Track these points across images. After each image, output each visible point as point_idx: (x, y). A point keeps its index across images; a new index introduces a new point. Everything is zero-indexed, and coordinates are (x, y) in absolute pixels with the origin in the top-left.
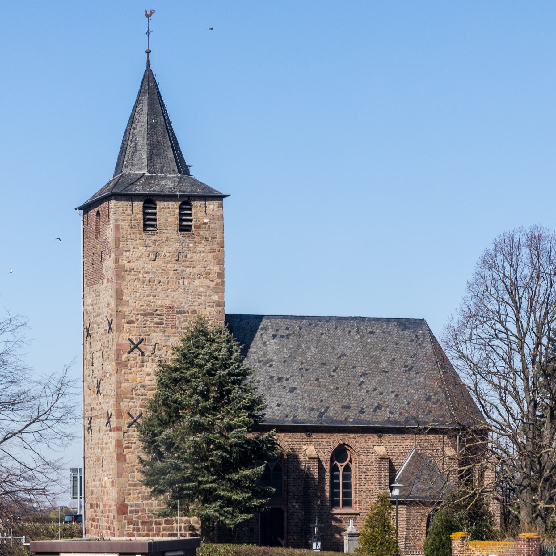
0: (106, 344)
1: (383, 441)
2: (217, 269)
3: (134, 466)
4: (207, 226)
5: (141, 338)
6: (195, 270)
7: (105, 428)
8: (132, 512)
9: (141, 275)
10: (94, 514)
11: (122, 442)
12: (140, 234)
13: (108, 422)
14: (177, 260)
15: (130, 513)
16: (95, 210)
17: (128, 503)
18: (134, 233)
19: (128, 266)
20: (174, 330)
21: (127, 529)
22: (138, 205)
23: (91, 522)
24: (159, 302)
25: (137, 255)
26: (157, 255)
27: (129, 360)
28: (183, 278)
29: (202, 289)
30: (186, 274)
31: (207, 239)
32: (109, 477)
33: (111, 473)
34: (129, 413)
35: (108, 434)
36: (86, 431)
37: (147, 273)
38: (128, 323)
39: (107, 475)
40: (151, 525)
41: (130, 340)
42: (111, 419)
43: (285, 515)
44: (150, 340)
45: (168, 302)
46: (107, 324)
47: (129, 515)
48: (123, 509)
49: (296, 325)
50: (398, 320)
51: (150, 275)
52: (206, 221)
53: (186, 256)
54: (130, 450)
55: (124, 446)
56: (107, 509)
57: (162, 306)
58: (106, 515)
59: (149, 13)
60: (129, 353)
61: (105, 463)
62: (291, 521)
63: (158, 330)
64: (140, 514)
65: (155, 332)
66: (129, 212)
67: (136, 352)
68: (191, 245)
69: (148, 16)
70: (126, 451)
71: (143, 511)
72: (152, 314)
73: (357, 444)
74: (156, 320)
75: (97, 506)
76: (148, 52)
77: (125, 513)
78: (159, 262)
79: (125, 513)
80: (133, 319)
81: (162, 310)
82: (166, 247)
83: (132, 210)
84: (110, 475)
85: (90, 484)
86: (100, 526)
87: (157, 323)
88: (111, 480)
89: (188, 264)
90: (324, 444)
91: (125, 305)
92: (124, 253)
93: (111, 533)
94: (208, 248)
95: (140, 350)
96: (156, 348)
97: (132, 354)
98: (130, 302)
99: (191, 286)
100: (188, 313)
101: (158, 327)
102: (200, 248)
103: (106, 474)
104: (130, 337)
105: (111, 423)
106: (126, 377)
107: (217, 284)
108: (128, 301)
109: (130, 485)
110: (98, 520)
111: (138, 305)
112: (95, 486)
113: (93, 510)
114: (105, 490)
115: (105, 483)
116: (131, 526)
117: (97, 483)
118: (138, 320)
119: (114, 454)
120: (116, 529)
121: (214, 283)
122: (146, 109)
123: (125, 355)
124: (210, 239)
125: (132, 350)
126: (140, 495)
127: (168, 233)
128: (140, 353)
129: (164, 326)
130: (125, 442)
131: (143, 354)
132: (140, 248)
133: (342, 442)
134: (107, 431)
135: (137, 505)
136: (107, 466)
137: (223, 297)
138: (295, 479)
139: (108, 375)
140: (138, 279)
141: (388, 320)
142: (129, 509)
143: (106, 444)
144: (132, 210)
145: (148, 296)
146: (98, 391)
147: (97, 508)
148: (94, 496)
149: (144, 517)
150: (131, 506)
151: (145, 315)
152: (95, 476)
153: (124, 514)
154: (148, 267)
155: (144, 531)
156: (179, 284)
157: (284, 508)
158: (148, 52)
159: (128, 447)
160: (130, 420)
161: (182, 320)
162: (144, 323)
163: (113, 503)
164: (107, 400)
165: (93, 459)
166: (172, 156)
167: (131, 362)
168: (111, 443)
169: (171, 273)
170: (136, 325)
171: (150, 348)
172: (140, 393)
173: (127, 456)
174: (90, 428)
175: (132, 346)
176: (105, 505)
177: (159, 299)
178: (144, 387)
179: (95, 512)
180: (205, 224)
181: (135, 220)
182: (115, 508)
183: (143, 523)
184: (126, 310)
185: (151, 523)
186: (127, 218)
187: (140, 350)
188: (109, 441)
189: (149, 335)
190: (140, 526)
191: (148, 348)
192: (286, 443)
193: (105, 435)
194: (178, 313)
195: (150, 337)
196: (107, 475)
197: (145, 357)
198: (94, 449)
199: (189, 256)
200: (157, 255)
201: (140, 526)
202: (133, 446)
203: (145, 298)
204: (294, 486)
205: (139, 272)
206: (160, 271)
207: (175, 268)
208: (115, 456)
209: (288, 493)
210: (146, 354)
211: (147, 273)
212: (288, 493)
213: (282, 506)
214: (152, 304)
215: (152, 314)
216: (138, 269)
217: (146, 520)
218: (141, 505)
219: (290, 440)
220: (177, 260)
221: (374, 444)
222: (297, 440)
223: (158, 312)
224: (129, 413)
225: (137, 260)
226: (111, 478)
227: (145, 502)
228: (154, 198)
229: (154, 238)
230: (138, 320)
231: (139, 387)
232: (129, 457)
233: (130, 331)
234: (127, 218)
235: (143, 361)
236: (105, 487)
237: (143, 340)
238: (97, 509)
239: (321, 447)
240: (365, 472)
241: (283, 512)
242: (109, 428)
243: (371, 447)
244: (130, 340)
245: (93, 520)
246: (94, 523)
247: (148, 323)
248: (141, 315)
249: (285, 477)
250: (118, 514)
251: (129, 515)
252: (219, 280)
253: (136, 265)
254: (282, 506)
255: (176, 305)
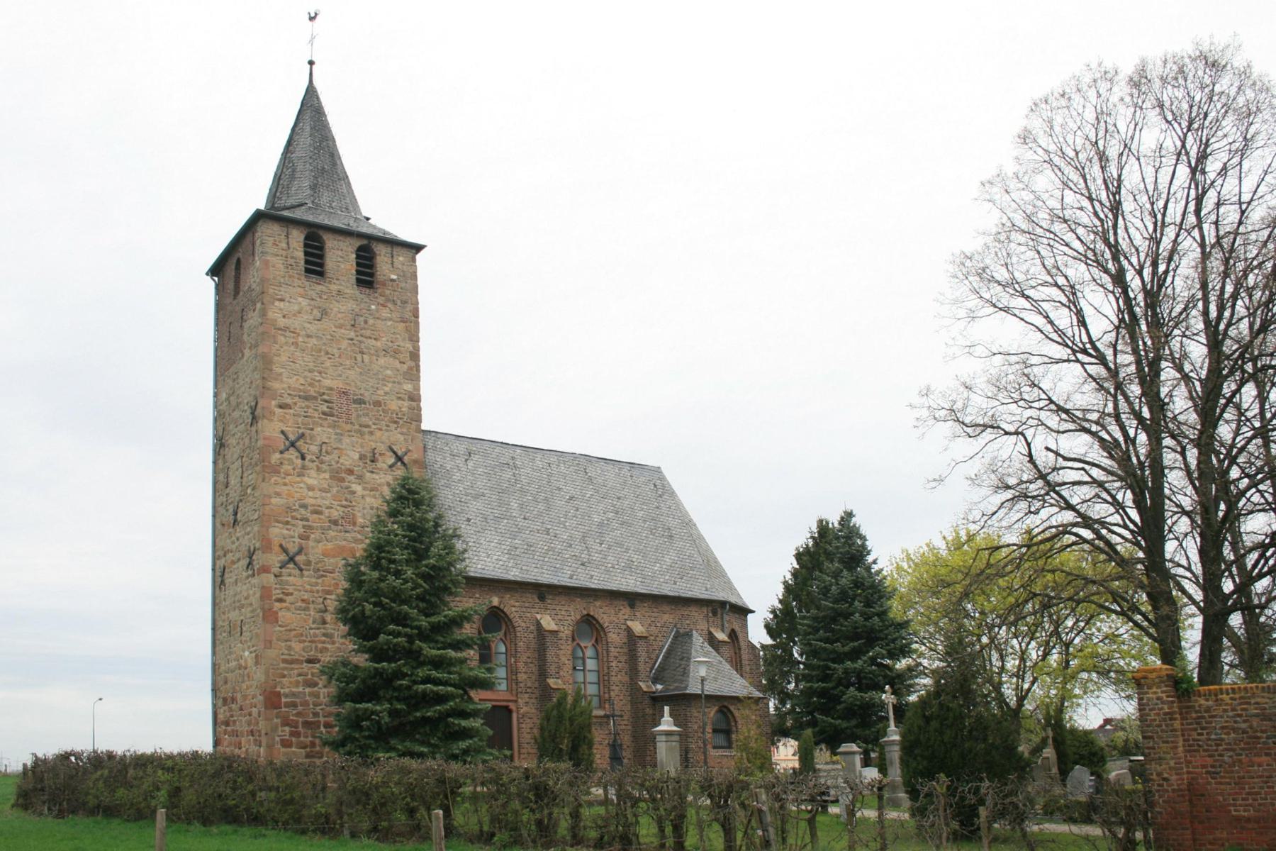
1: (637, 613)
2: (409, 346)
3: (290, 630)
4: (395, 284)
6: (379, 344)
7: (245, 574)
8: (287, 705)
9: (301, 339)
11: (271, 591)
12: (299, 279)
13: (250, 564)
14: (353, 326)
15: (285, 707)
17: (282, 691)
18: (290, 276)
19: (282, 322)
20: (349, 427)
22: (298, 237)
23: (224, 727)
24: (327, 383)
26: (324, 313)
27: (281, 463)
28: (362, 353)
29: (389, 372)
30: (366, 348)
31: (394, 302)
34: (281, 546)
36: (217, 589)
37: (309, 336)
38: (281, 407)
39: (249, 648)
40: (319, 727)
41: (283, 432)
42: (254, 557)
43: (515, 716)
44: (312, 437)
47: (284, 709)
51: (314, 341)
52: (394, 277)
53: (366, 322)
54: (284, 605)
57: (331, 389)
59: (313, 15)
60: (281, 452)
61: (244, 629)
62: (523, 726)
63: (325, 423)
64: (300, 708)
65: (321, 425)
66: (284, 245)
68: (373, 307)
69: (312, 19)
70: (277, 605)
71: (305, 704)
72: (315, 398)
73: (605, 616)
74: (324, 408)
75: (233, 700)
76: (311, 63)
77: (278, 706)
78: (326, 323)
79: (278, 706)
80: (289, 401)
82: (337, 305)
83: (288, 244)
85: (223, 668)
87: (324, 413)
88: (254, 655)
89: (368, 333)
90: (563, 613)
91: (276, 379)
92: (277, 303)
93: (256, 740)
95: (299, 451)
96: (324, 450)
97: (286, 455)
98: (285, 375)
99: (373, 366)
103: (246, 646)
104: (284, 429)
107: (410, 368)
108: (281, 374)
109: (285, 661)
110: (234, 722)
111: (295, 382)
113: (226, 708)
114: (246, 672)
115: (246, 661)
116: (287, 729)
118: (295, 404)
119: (259, 611)
120: (263, 732)
121: (405, 366)
122: (308, 129)
123: (277, 456)
124: (399, 303)
126: (300, 679)
127: (341, 285)
128: (297, 454)
130: (278, 591)
132: (300, 299)
133: (585, 612)
136: (248, 634)
137: (417, 388)
138: (526, 663)
140: (295, 344)
142: (284, 700)
144: (288, 244)
148: (229, 685)
151: (306, 398)
152: (230, 653)
153: (276, 708)
154: (312, 328)
155: (307, 737)
156: (356, 360)
157: (512, 706)
158: (311, 63)
159: (280, 600)
160: (283, 557)
161: (361, 413)
163: (258, 692)
164: (249, 529)
165: (227, 628)
167: (286, 467)
170: (292, 411)
171: (314, 449)
172: (299, 517)
173: (280, 614)
174: (222, 582)
176: (245, 697)
178: (304, 506)
180: (393, 280)
181: (292, 258)
182: (261, 698)
183: (307, 724)
184: (276, 385)
186: (281, 252)
189: (312, 429)
190: (300, 729)
192: (513, 609)
194: (355, 402)
197: (307, 463)
199: (371, 321)
200: (324, 313)
201: (300, 729)
202: (289, 599)
203: (306, 373)
204: (525, 673)
205: (299, 335)
206: (329, 337)
207: (350, 337)
208: (261, 614)
209: (517, 684)
210: (308, 457)
212: (517, 684)
213: (510, 704)
215: (315, 398)
217: (311, 719)
219: (517, 604)
220: (353, 326)
221: (626, 617)
222: (527, 605)
224: (281, 546)
225: (294, 315)
227: (307, 690)
228: (321, 233)
229: (319, 288)
230: (295, 404)
231: (297, 507)
234: (281, 252)
235: (303, 467)
236: (246, 668)
237: (303, 435)
238: (234, 706)
239: (560, 617)
240: (616, 657)
241: (510, 711)
243: (623, 621)
244: (283, 432)
245: (227, 724)
246: (229, 729)
247: (310, 410)
248: (300, 397)
249: (513, 660)
250: (266, 708)
251: (284, 709)
252: (413, 364)
253: (295, 323)
254: (510, 704)
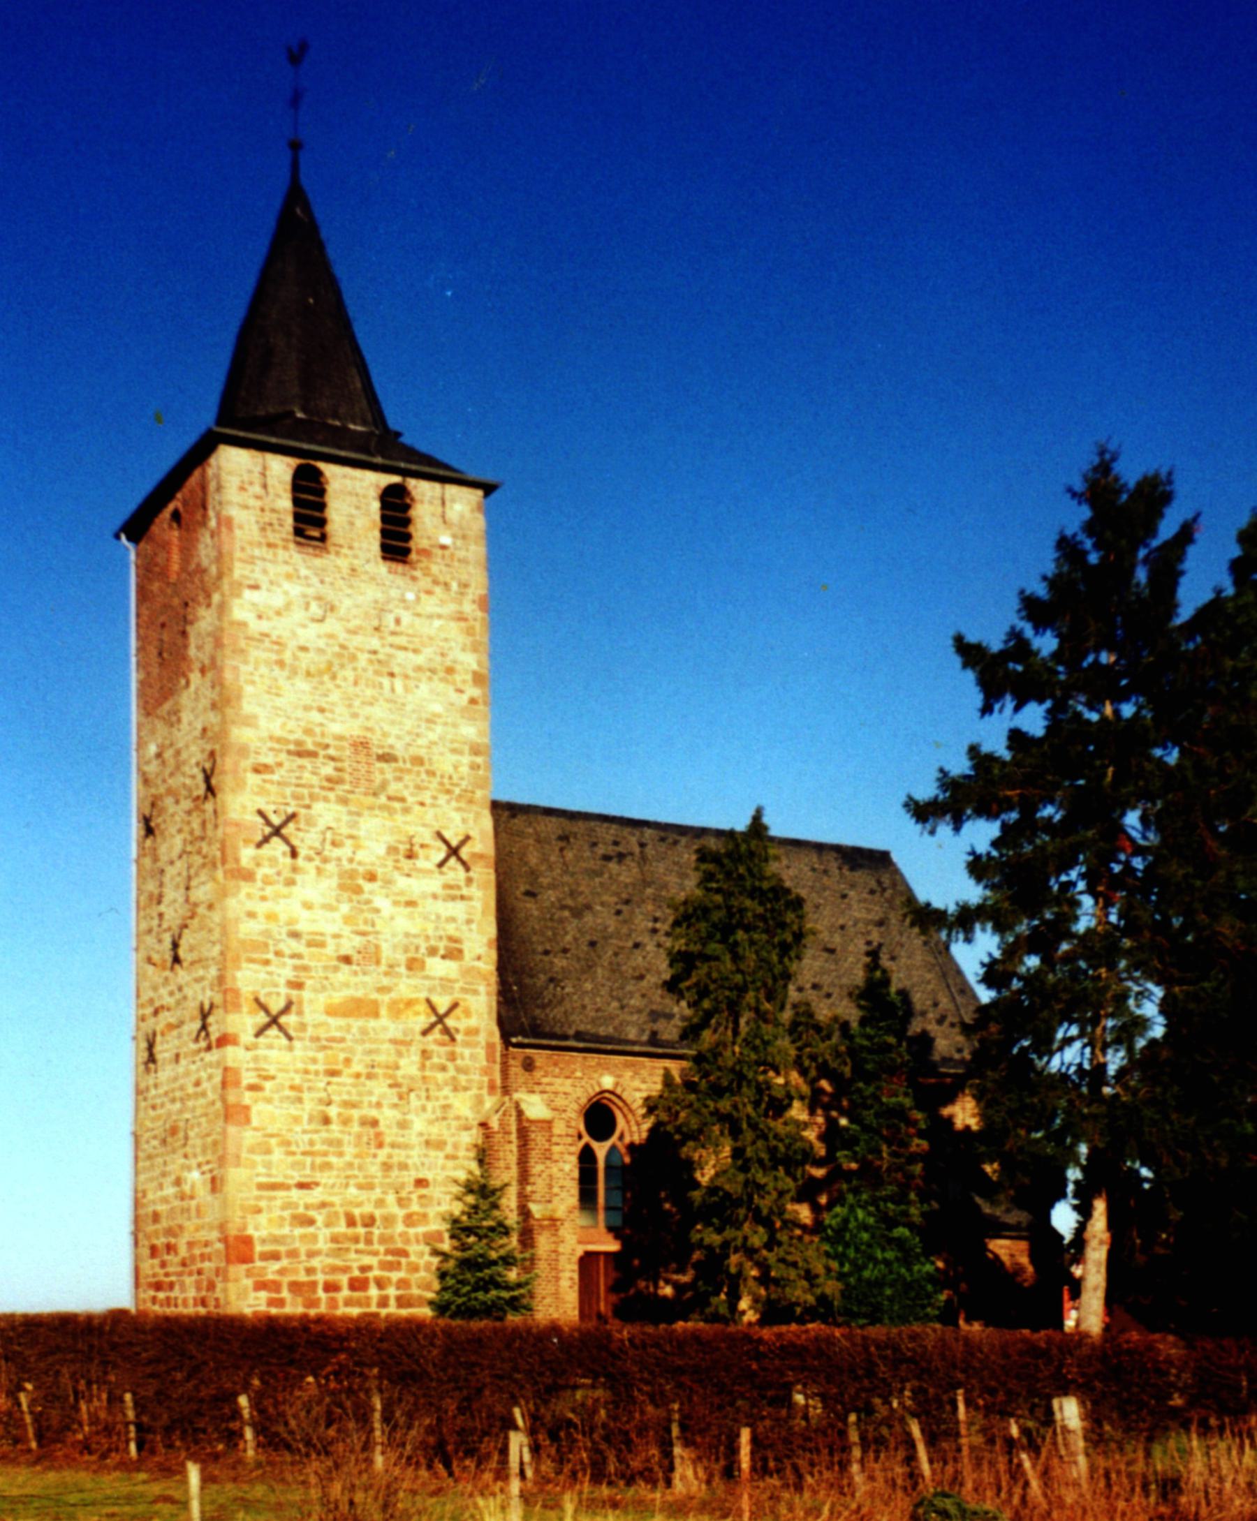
0: (198, 833)
4: (447, 553)
5: (290, 810)
7: (193, 1046)
8: (267, 1257)
10: (161, 1272)
14: (377, 629)
16: (167, 513)
19: (255, 626)
21: (252, 1302)
24: (336, 728)
25: (278, 601)
28: (392, 675)
32: (206, 1168)
33: (209, 1157)
34: (257, 1000)
35: (202, 1060)
39: (199, 1165)
41: (261, 813)
42: (211, 1019)
45: (352, 729)
46: (200, 777)
48: (242, 1247)
49: (631, 840)
50: (838, 849)
53: (398, 621)
54: (260, 1094)
55: (245, 1082)
56: (197, 1252)
57: (340, 738)
58: (194, 1268)
60: (259, 845)
63: (331, 795)
65: (326, 799)
67: (277, 847)
80: (269, 759)
81: (337, 748)
84: (208, 1162)
85: (150, 1196)
86: (176, 1299)
87: (329, 779)
88: (208, 1176)
94: (451, 608)
95: (286, 841)
97: (266, 850)
100: (404, 761)
101: (331, 789)
102: (429, 605)
103: (193, 1162)
105: (211, 1029)
106: (250, 906)
112: (165, 1200)
113: (156, 1262)
114: (193, 1203)
115: (193, 1187)
117: (170, 1191)
118: (280, 765)
125: (266, 840)
127: (356, 557)
129: (347, 787)
131: (294, 854)
134: (199, 1051)
135: (276, 1240)
139: (201, 910)
140: (281, 664)
141: (820, 848)
142: (258, 1248)
143: (197, 1084)
145: (307, 708)
146: (176, 960)
147: (168, 1253)
149: (295, 1271)
150: (263, 1241)
152: (164, 1174)
159: (253, 1088)
162: (297, 774)
166: (359, 385)
168: (210, 1077)
169: (363, 658)
170: (275, 777)
175: (268, 830)
177: (333, 720)
179: (163, 1265)
180: (444, 547)
185: (313, 1285)
187: (286, 841)
188: (203, 1075)
191: (306, 840)
193: (194, 1062)
195: (313, 812)
196: (199, 1165)
197: (300, 861)
198: (162, 1105)
202: (268, 1085)
211: (304, 649)
214: (318, 730)
216: (279, 637)
217: (303, 1277)
218: (289, 1240)
223: (331, 752)
226: (211, 1171)
232: (259, 1113)
233: (261, 791)
235: (295, 869)
242: (203, 1044)
244: (261, 813)
245: (158, 1286)
253: (278, 627)
255: (375, 739)
